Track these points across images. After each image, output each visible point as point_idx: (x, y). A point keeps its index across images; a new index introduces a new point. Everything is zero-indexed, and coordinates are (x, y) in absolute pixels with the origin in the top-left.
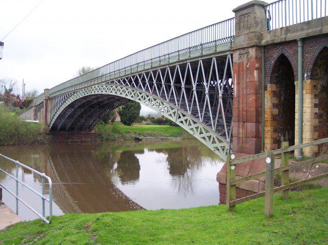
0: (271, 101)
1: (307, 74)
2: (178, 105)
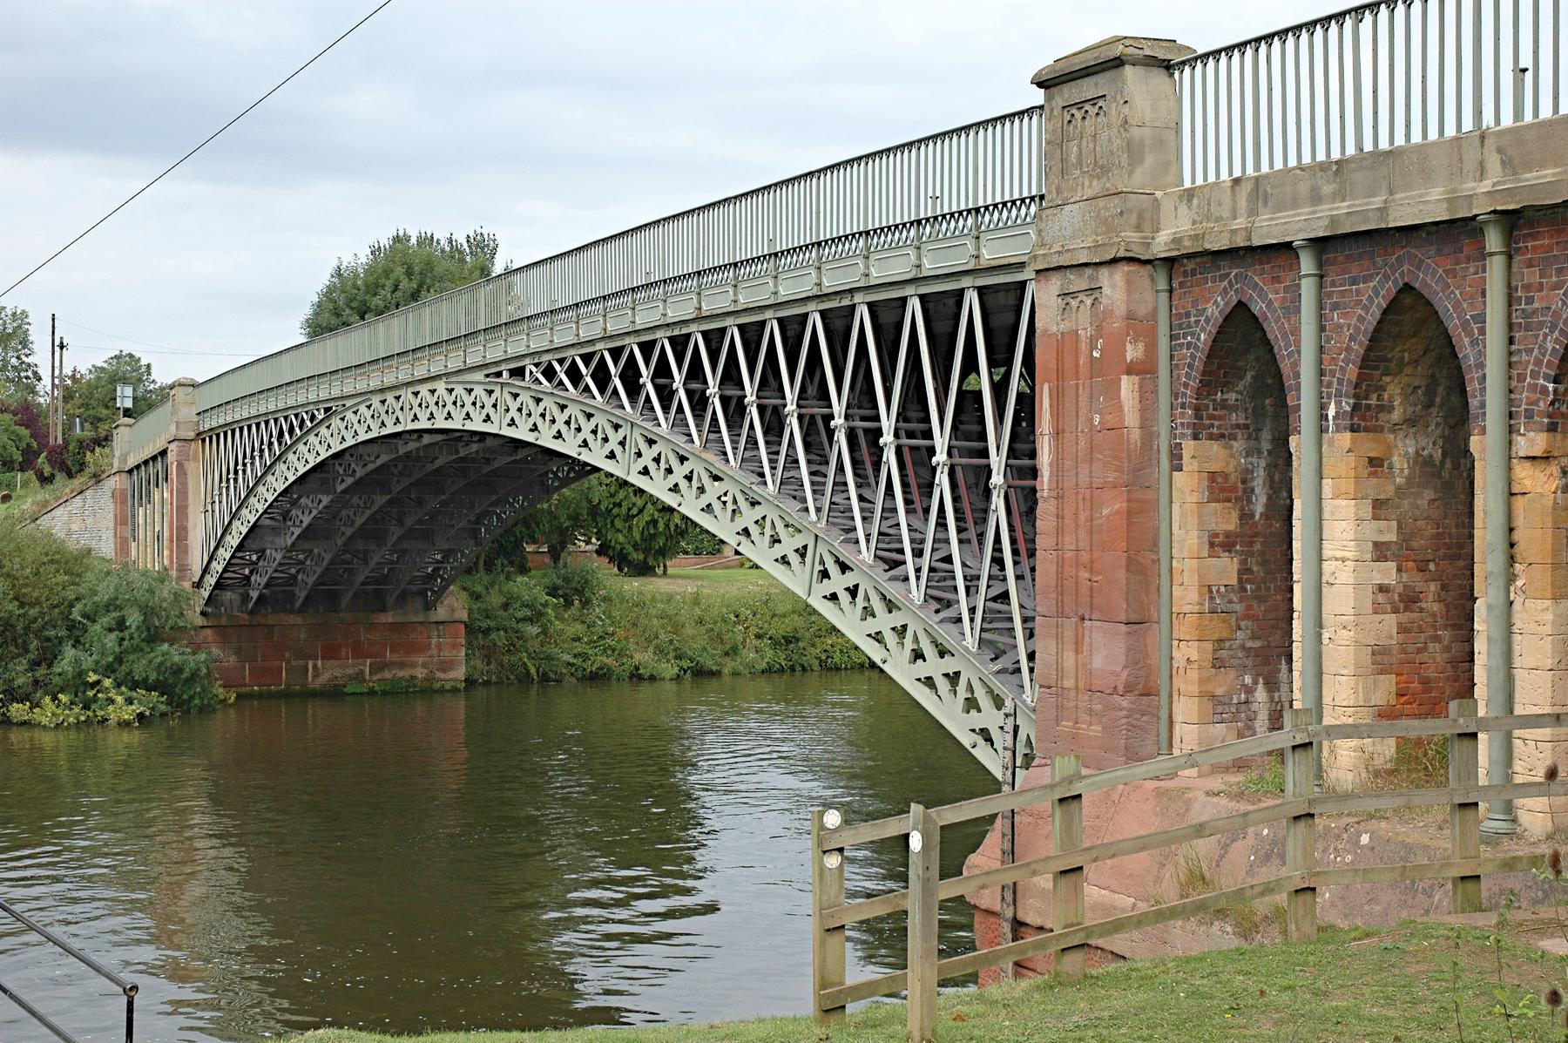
0: (1201, 523)
1: (1338, 404)
2: (818, 510)
